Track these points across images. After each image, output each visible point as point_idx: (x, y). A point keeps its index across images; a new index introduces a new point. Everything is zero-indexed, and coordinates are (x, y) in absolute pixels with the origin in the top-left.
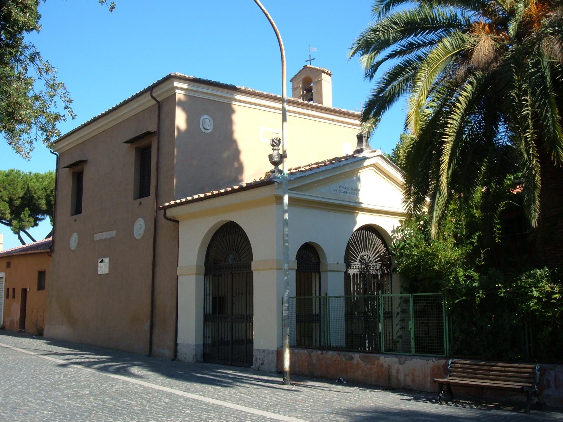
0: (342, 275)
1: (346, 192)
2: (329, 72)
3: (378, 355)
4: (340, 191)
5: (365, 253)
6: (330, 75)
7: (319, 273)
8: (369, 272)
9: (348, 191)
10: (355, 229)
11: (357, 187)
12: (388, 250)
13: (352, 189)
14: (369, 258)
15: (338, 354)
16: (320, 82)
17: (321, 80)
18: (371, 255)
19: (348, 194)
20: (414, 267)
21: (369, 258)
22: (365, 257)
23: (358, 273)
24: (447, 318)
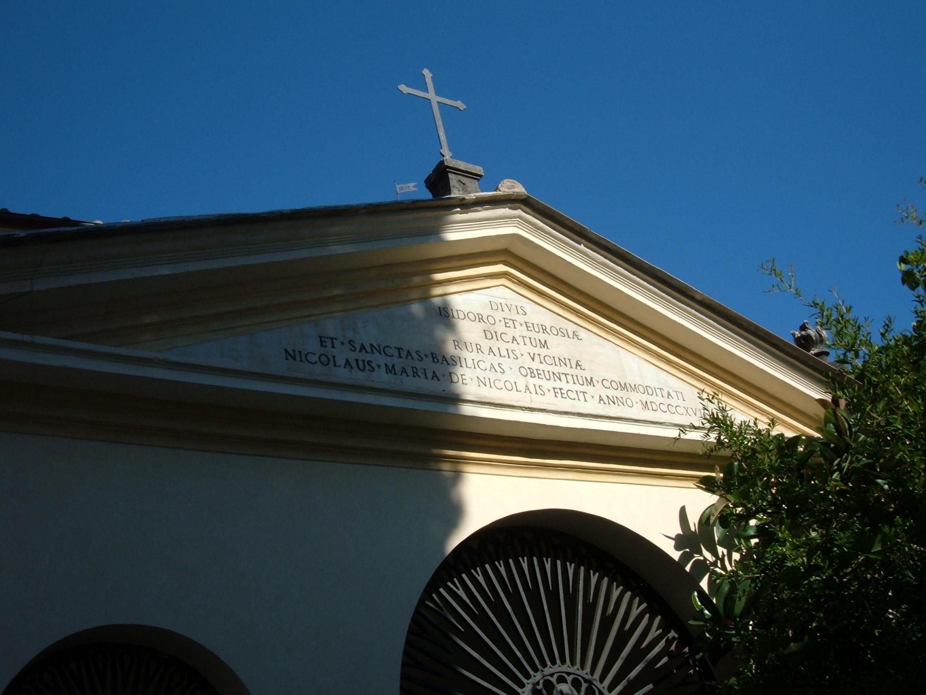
1: (367, 366)
4: (328, 361)
9: (379, 359)
12: (686, 637)
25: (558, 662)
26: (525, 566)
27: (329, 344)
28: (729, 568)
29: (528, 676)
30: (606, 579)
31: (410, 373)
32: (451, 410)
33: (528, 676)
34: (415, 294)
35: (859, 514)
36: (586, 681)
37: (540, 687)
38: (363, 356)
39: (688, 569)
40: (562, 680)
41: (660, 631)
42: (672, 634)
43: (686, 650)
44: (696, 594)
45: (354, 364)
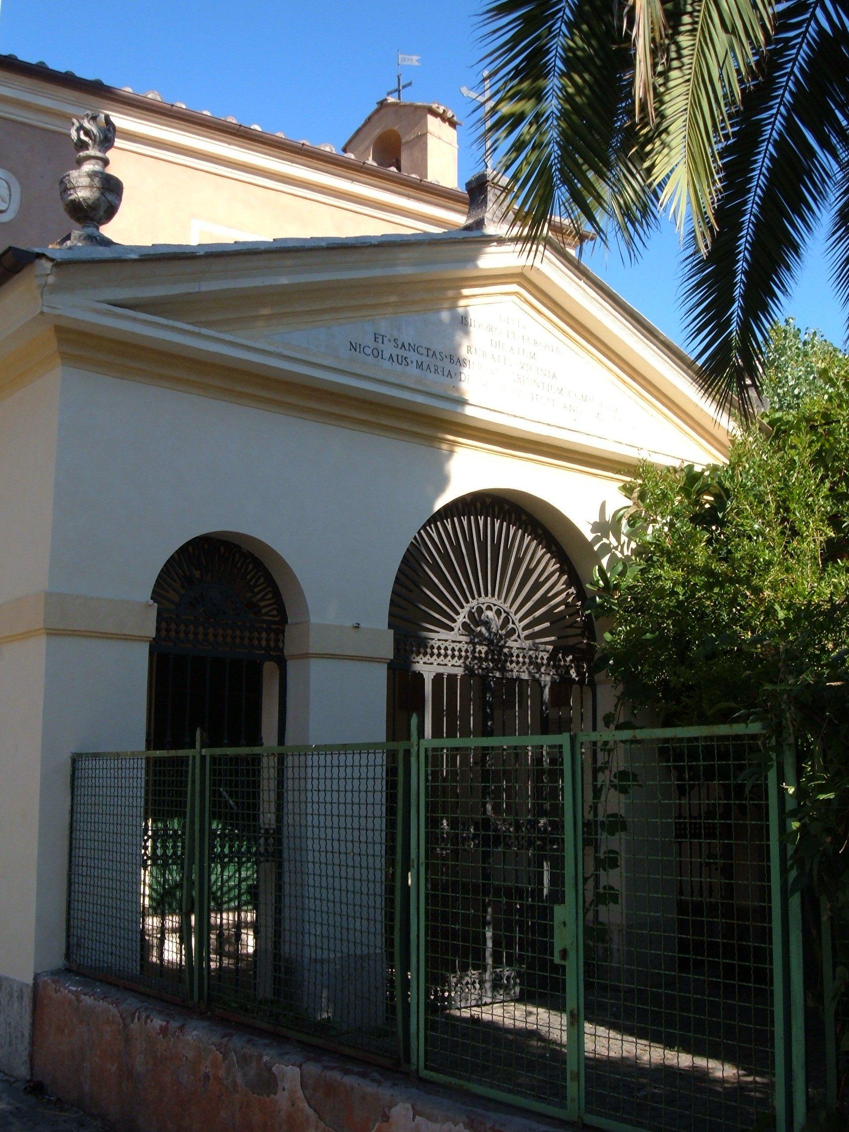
0: (380, 674)
1: (404, 361)
2: (450, 114)
3: (385, 1092)
4: (378, 354)
5: (489, 600)
6: (453, 124)
7: (282, 663)
8: (503, 670)
9: (413, 356)
10: (440, 503)
11: (456, 348)
12: (581, 594)
13: (431, 353)
14: (506, 621)
15: (219, 1046)
16: (422, 139)
17: (425, 135)
18: (511, 610)
19: (412, 370)
20: (661, 641)
21: (506, 621)
22: (490, 614)
23: (460, 672)
24: (795, 901)
25: (490, 595)
26: (481, 523)
27: (380, 340)
28: (626, 553)
29: (468, 602)
30: (520, 531)
31: (433, 369)
32: (459, 409)
33: (468, 602)
34: (447, 304)
35: (249, 942)
36: (505, 612)
37: (473, 611)
38: (402, 352)
39: (596, 548)
40: (489, 608)
41: (564, 586)
42: (570, 591)
43: (579, 603)
44: (597, 567)
45: (395, 359)
